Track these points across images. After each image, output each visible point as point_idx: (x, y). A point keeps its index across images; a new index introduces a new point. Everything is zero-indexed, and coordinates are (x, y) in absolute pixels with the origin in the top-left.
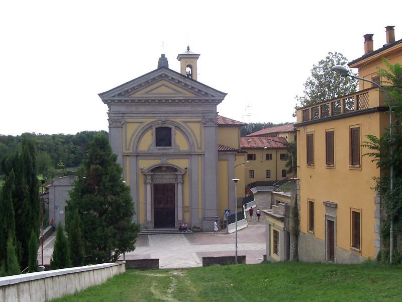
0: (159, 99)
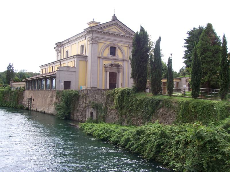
0: (115, 33)
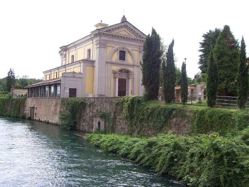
0: (124, 36)
